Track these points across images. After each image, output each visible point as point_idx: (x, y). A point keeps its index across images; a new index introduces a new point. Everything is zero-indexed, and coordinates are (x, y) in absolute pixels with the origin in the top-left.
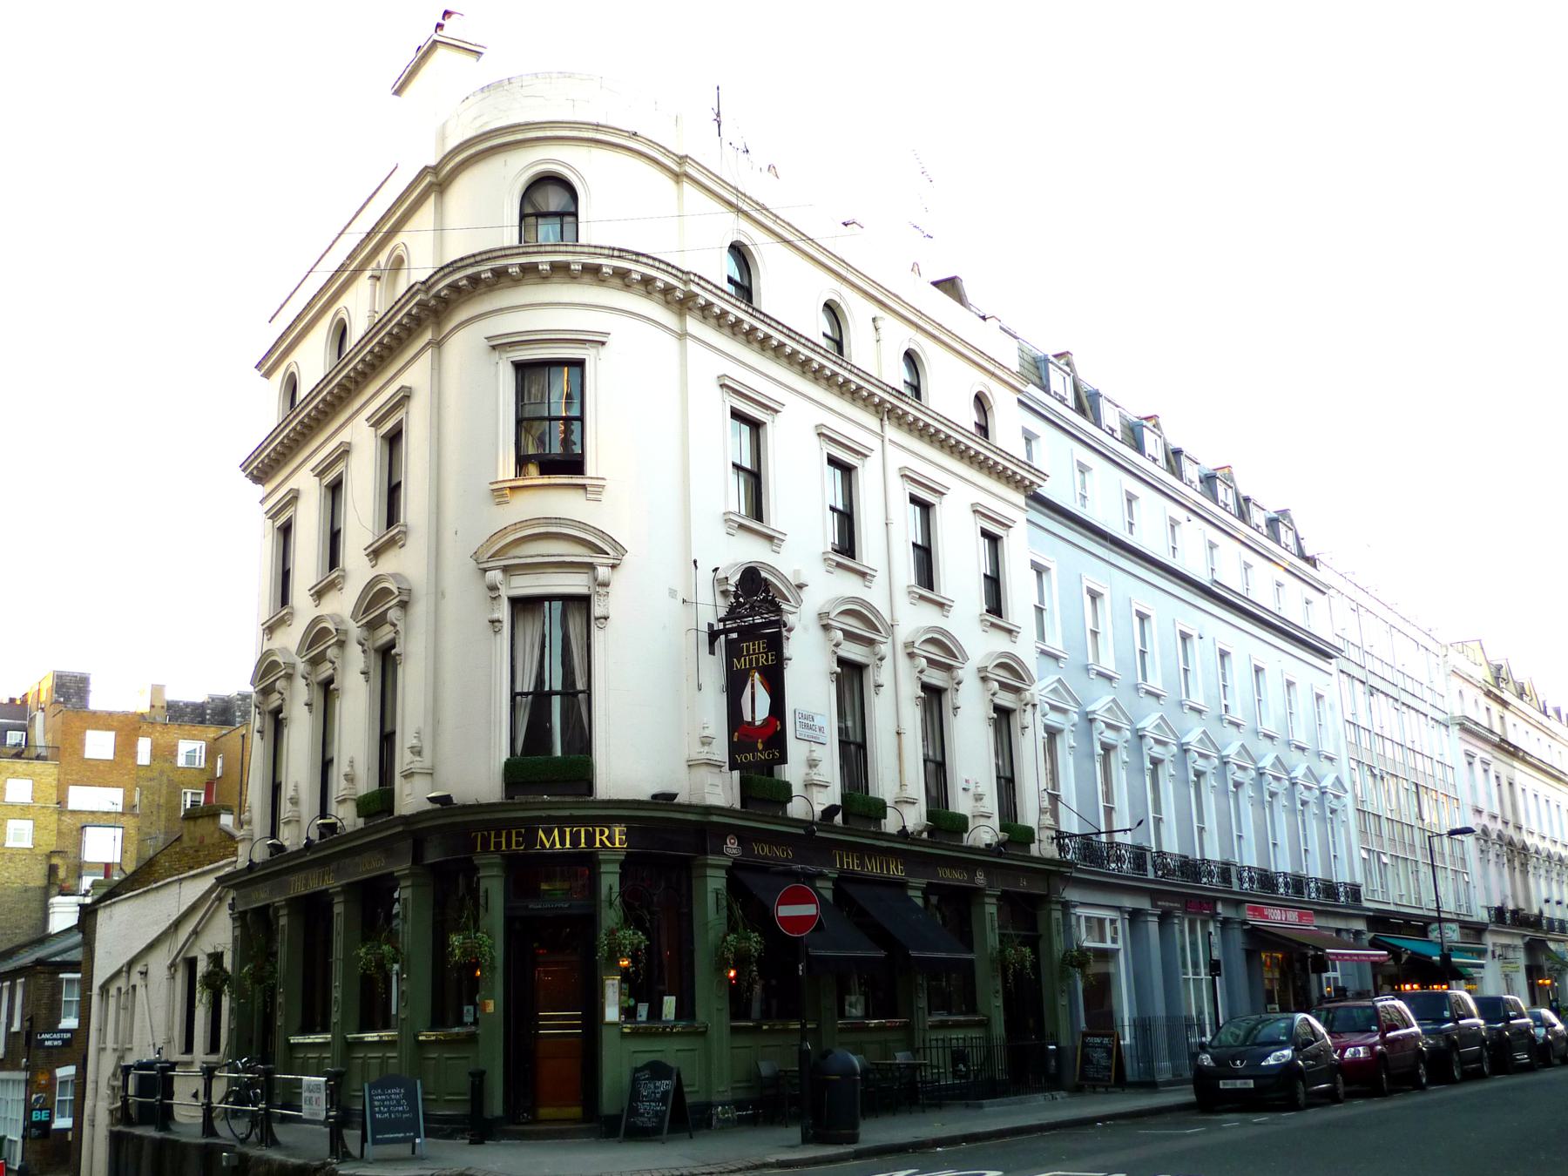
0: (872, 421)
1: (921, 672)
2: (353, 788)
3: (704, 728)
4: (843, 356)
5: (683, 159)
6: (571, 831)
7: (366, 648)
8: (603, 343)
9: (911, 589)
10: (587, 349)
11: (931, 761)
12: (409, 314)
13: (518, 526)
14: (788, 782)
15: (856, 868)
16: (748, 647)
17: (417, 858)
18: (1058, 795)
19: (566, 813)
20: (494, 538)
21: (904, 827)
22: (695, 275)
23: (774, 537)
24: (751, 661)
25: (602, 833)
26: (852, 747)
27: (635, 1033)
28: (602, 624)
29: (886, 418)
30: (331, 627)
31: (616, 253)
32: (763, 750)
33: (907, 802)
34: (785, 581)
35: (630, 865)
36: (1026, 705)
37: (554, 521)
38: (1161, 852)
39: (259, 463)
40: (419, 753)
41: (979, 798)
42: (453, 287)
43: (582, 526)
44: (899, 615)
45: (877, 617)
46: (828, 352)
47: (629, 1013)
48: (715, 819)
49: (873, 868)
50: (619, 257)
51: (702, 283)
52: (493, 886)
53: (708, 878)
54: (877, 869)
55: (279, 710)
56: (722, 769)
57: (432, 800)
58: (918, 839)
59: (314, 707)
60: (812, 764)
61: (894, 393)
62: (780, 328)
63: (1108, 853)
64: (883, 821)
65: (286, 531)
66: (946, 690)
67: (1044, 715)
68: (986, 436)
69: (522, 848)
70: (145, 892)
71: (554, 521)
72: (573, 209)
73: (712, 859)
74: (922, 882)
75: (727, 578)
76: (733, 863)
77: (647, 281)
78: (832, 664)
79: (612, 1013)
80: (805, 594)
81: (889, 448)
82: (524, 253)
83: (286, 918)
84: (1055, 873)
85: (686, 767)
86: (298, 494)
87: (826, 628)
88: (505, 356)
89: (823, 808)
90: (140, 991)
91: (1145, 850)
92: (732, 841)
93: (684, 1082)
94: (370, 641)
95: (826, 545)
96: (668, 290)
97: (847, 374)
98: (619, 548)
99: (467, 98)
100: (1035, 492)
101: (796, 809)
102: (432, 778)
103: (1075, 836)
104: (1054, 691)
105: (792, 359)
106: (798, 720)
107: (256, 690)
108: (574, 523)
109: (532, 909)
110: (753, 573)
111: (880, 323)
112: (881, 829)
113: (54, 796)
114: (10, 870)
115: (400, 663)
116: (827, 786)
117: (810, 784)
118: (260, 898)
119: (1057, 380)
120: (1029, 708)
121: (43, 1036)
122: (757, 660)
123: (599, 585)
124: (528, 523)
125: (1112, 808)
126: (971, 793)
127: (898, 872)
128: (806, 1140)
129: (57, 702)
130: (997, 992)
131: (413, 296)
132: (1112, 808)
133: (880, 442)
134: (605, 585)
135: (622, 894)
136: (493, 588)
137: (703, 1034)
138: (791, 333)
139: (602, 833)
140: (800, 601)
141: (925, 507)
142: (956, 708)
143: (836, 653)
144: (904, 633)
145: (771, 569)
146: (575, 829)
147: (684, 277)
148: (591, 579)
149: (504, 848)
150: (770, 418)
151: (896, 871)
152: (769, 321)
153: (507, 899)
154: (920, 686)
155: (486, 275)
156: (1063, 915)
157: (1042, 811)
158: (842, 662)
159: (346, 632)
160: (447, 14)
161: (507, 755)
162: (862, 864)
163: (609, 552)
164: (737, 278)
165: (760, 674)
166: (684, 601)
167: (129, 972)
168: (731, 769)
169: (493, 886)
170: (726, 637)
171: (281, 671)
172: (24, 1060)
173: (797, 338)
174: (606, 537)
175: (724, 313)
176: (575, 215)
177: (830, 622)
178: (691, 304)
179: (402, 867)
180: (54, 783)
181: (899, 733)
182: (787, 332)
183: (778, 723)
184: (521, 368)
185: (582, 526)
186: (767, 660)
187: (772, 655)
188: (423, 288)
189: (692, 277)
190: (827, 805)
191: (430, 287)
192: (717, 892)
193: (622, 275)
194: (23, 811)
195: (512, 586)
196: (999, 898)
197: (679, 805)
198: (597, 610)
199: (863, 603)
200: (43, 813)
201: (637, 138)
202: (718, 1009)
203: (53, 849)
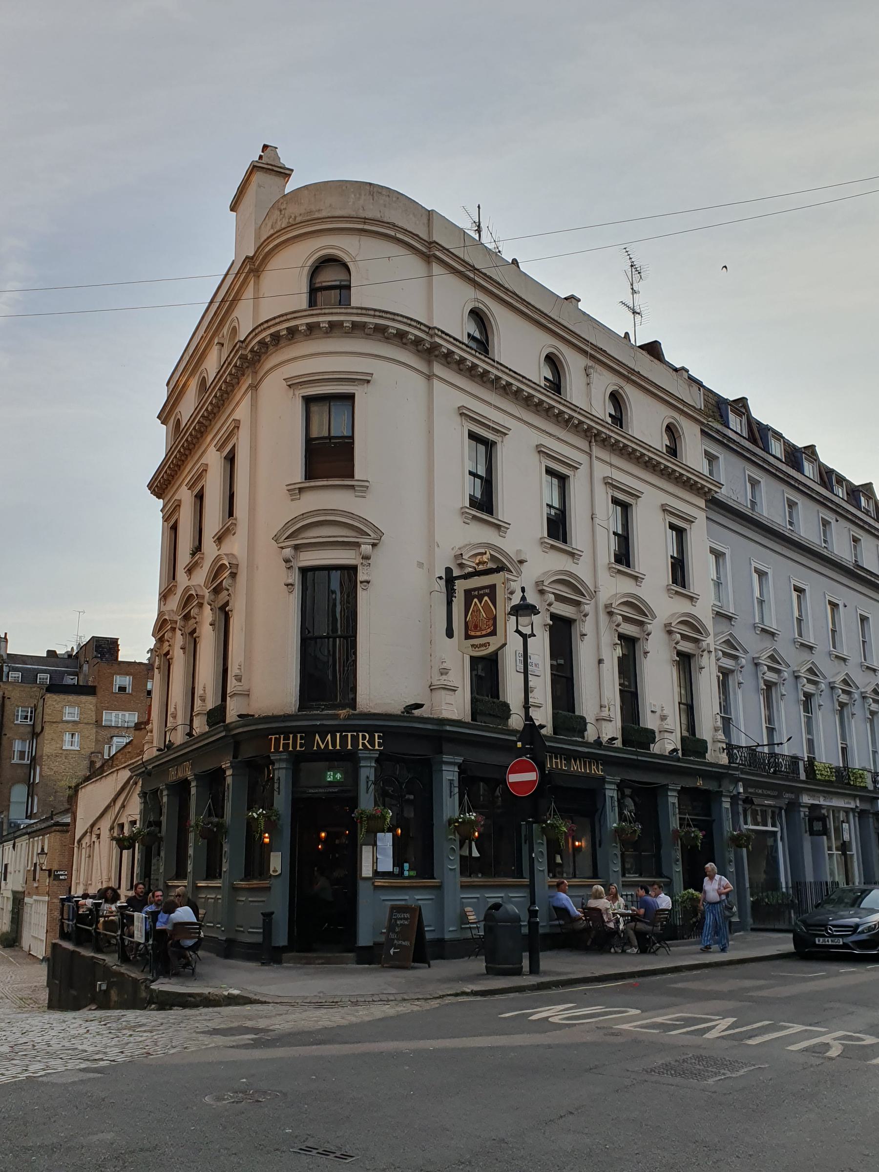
0: (583, 444)
3: (442, 662)
4: (560, 394)
8: (368, 381)
10: (356, 385)
11: (683, 704)
15: (564, 768)
18: (731, 718)
21: (599, 738)
22: (439, 330)
28: (366, 586)
29: (593, 440)
30: (193, 593)
36: (703, 651)
38: (775, 753)
41: (663, 718)
42: (262, 343)
48: (448, 728)
52: (281, 773)
53: (444, 772)
55: (167, 653)
63: (768, 761)
65: (174, 528)
67: (718, 660)
68: (486, 352)
74: (618, 779)
75: (462, 554)
76: (463, 761)
77: (401, 336)
80: (524, 568)
81: (596, 463)
84: (718, 775)
86: (181, 503)
87: (670, 632)
88: (297, 393)
90: (97, 844)
91: (799, 759)
93: (425, 923)
95: (542, 532)
96: (418, 342)
100: (713, 497)
101: (591, 734)
103: (742, 747)
104: (727, 642)
113: (94, 717)
114: (65, 764)
119: (808, 468)
120: (705, 653)
125: (773, 729)
126: (658, 714)
127: (599, 772)
129: (96, 657)
130: (678, 860)
132: (773, 729)
136: (287, 561)
138: (641, 443)
139: (364, 738)
140: (520, 572)
141: (625, 508)
142: (646, 653)
143: (549, 610)
144: (604, 597)
146: (344, 734)
148: (358, 553)
149: (291, 749)
150: (500, 439)
151: (597, 770)
154: (617, 636)
156: (731, 805)
157: (716, 730)
159: (203, 597)
164: (477, 335)
167: (91, 833)
169: (281, 773)
174: (369, 524)
175: (463, 360)
177: (545, 588)
178: (437, 353)
191: (247, 346)
192: (451, 782)
193: (380, 330)
196: (679, 792)
198: (361, 577)
199: (571, 574)
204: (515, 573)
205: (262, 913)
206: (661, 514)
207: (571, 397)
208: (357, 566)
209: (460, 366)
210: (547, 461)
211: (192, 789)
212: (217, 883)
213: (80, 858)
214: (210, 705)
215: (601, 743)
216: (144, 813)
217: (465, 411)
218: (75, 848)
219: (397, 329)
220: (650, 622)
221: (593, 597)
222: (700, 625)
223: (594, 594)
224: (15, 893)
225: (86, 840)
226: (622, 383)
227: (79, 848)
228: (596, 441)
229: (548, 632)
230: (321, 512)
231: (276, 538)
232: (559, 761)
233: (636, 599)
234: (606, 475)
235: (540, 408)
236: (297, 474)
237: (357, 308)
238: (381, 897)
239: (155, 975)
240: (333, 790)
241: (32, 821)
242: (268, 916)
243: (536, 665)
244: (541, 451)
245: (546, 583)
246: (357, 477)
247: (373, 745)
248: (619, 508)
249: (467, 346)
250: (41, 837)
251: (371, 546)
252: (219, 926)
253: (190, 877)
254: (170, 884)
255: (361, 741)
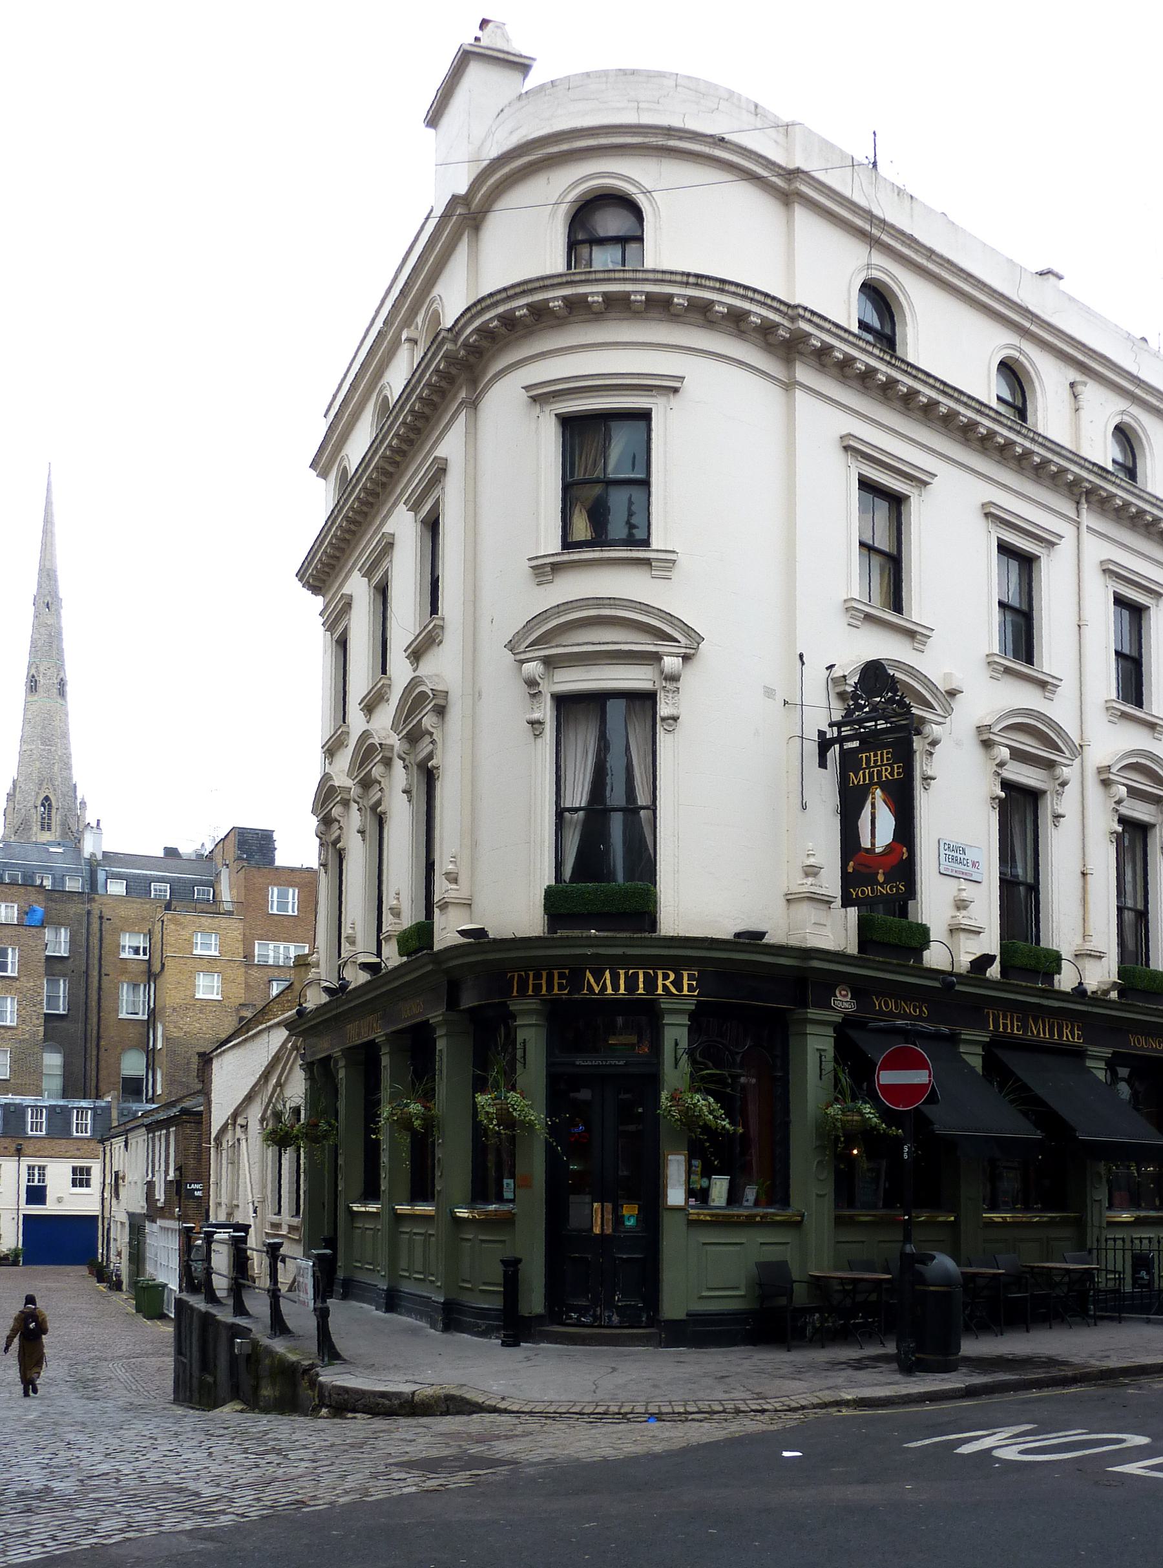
0: (1067, 508)
1: (1119, 802)
2: (399, 924)
5: (794, 174)
6: (626, 974)
7: (407, 762)
8: (676, 390)
9: (1109, 705)
12: (437, 371)
13: (562, 608)
14: (925, 925)
15: (1015, 1032)
16: (868, 759)
17: (452, 1003)
19: (619, 951)
20: (532, 624)
21: (1081, 984)
22: (805, 309)
23: (916, 632)
24: (871, 775)
25: (666, 977)
26: (1022, 888)
27: (720, 1222)
31: (692, 280)
32: (884, 882)
33: (1090, 955)
34: (930, 685)
35: (699, 1018)
37: (607, 602)
39: (312, 571)
40: (455, 881)
43: (643, 607)
44: (1089, 734)
45: (1059, 735)
46: (1000, 414)
47: (699, 1195)
48: (816, 964)
49: (1040, 1032)
50: (696, 284)
51: (815, 319)
54: (1044, 1033)
56: (832, 906)
57: (463, 933)
58: (1104, 1000)
59: (367, 835)
60: (961, 905)
61: (1095, 469)
62: (931, 381)
64: (1057, 977)
66: (1154, 826)
69: (566, 992)
70: (245, 1040)
71: (607, 602)
72: (639, 234)
73: (813, 1013)
74: (1107, 1052)
78: (994, 788)
79: (676, 1196)
80: (958, 703)
81: (1086, 536)
82: (568, 283)
83: (344, 1069)
85: (785, 903)
87: (987, 744)
88: (547, 409)
89: (973, 957)
90: (243, 1143)
92: (844, 993)
94: (412, 756)
95: (990, 644)
97: (1028, 444)
98: (693, 634)
99: (502, 111)
102: (470, 908)
105: (948, 423)
106: (942, 852)
107: (319, 818)
108: (634, 605)
109: (579, 1066)
110: (877, 669)
111: (1079, 388)
112: (1053, 985)
113: (241, 950)
114: (200, 1021)
115: (438, 777)
116: (980, 932)
117: (957, 929)
118: (326, 1046)
121: (193, 1186)
122: (879, 773)
123: (666, 679)
124: (574, 605)
127: (1073, 1038)
128: (908, 1368)
129: (239, 858)
131: (439, 348)
133: (1075, 529)
134: (674, 678)
135: (691, 1053)
136: (531, 683)
137: (798, 1225)
138: (946, 389)
139: (666, 977)
140: (950, 710)
142: (1058, 816)
143: (999, 774)
145: (897, 664)
146: (631, 971)
147: (790, 312)
148: (657, 672)
149: (544, 992)
151: (1071, 1036)
152: (914, 372)
153: (550, 1053)
154: (1116, 819)
155: (522, 312)
158: (1006, 785)
160: (484, 23)
161: (549, 879)
162: (1025, 1027)
163: (680, 639)
165: (882, 790)
166: (786, 703)
167: (234, 1124)
168: (845, 905)
170: (841, 747)
171: (337, 797)
172: (178, 1209)
173: (956, 395)
176: (640, 239)
177: (992, 737)
179: (436, 1016)
180: (240, 937)
181: (1084, 874)
182: (941, 387)
183: (904, 849)
184: (567, 422)
185: (643, 607)
186: (892, 774)
187: (898, 768)
188: (450, 335)
189: (801, 312)
190: (978, 954)
191: (459, 334)
193: (736, 322)
194: (210, 965)
195: (555, 681)
197: (767, 946)
198: (664, 710)
199: (1041, 716)
200: (231, 967)
201: (725, 145)
202: (818, 1195)
203: (242, 1001)
204: (1068, 755)
205: (503, 1261)
206: (981, 524)
207: (1036, 425)
208: (657, 691)
209: (843, 369)
210: (999, 530)
211: (383, 1058)
212: (372, 1208)
213: (219, 1168)
214: (407, 922)
215: (1085, 991)
216: (313, 1095)
217: (852, 443)
218: (212, 1149)
219: (730, 307)
220: (940, 720)
221: (1077, 754)
222: (1049, 726)
223: (1079, 750)
224: (131, 1216)
225: (229, 1135)
226: (1135, 410)
227: (217, 1148)
228: (1087, 501)
229: (1115, 844)
230: (591, 602)
231: (511, 646)
232: (1009, 1022)
233: (1037, 719)
234: (844, 433)
235: (985, 444)
236: (551, 543)
237: (654, 271)
238: (758, 1239)
239: (326, 1359)
240: (617, 1063)
241: (154, 1106)
242: (512, 1267)
243: (974, 864)
244: (991, 515)
245: (996, 729)
246: (654, 546)
247: (680, 989)
248: (1126, 613)
249: (997, 412)
250: (164, 1132)
251: (680, 659)
252: (434, 1279)
253: (384, 1197)
254: (355, 1209)
255: (660, 982)
